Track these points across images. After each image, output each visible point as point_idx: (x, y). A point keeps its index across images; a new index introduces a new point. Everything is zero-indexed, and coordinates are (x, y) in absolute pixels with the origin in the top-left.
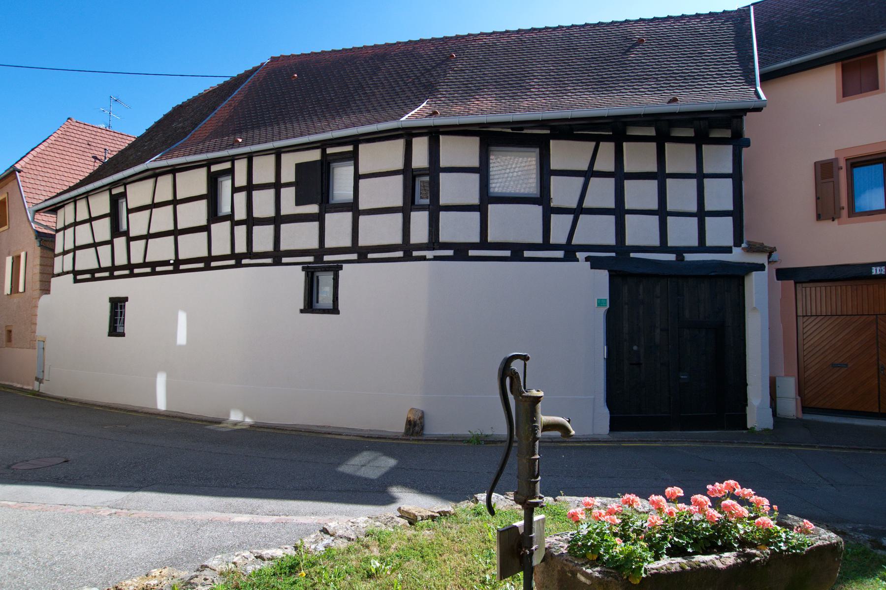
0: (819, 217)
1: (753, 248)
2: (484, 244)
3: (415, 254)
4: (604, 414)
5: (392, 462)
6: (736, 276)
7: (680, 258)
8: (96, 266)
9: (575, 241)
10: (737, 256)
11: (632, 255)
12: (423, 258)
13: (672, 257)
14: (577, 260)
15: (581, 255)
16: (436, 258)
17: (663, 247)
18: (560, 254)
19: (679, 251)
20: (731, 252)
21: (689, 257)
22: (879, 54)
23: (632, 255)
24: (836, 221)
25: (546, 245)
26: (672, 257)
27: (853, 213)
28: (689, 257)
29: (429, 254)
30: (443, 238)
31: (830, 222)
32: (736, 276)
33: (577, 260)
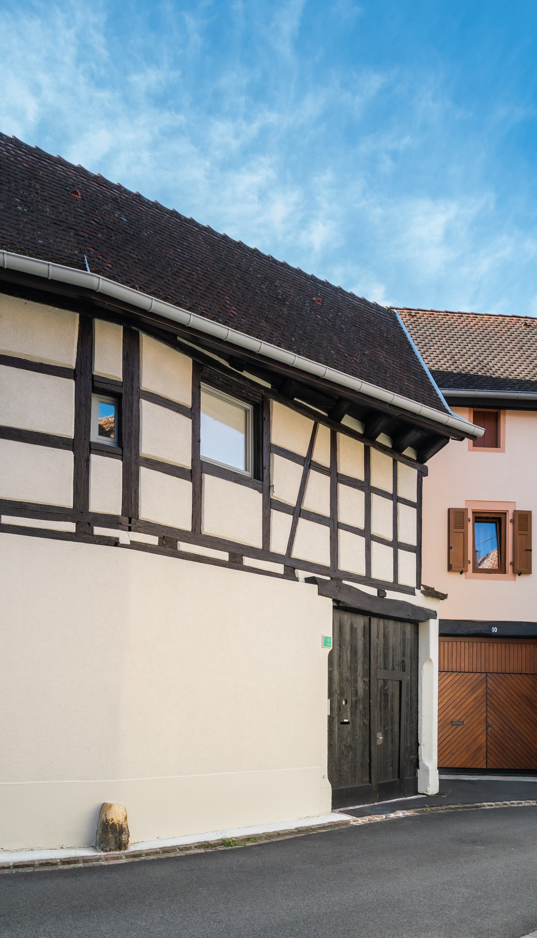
0: (450, 568)
1: (430, 593)
2: (196, 535)
3: (98, 531)
4: (325, 790)
5: (390, 446)
6: (416, 619)
7: (381, 594)
8: (390, 579)
9: (209, 480)
10: (418, 600)
11: (345, 582)
12: (115, 543)
13: (373, 591)
14: (297, 580)
15: (301, 574)
16: (135, 546)
17: (367, 580)
18: (279, 568)
19: (382, 586)
20: (414, 594)
21: (391, 595)
22: (502, 411)
23: (345, 582)
24: (463, 574)
25: (264, 553)
26: (373, 591)
27: (476, 570)
28: (391, 595)
29: (125, 537)
30: (146, 513)
31: (459, 574)
32: (416, 619)
33: (297, 580)
